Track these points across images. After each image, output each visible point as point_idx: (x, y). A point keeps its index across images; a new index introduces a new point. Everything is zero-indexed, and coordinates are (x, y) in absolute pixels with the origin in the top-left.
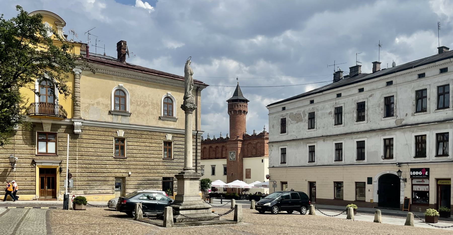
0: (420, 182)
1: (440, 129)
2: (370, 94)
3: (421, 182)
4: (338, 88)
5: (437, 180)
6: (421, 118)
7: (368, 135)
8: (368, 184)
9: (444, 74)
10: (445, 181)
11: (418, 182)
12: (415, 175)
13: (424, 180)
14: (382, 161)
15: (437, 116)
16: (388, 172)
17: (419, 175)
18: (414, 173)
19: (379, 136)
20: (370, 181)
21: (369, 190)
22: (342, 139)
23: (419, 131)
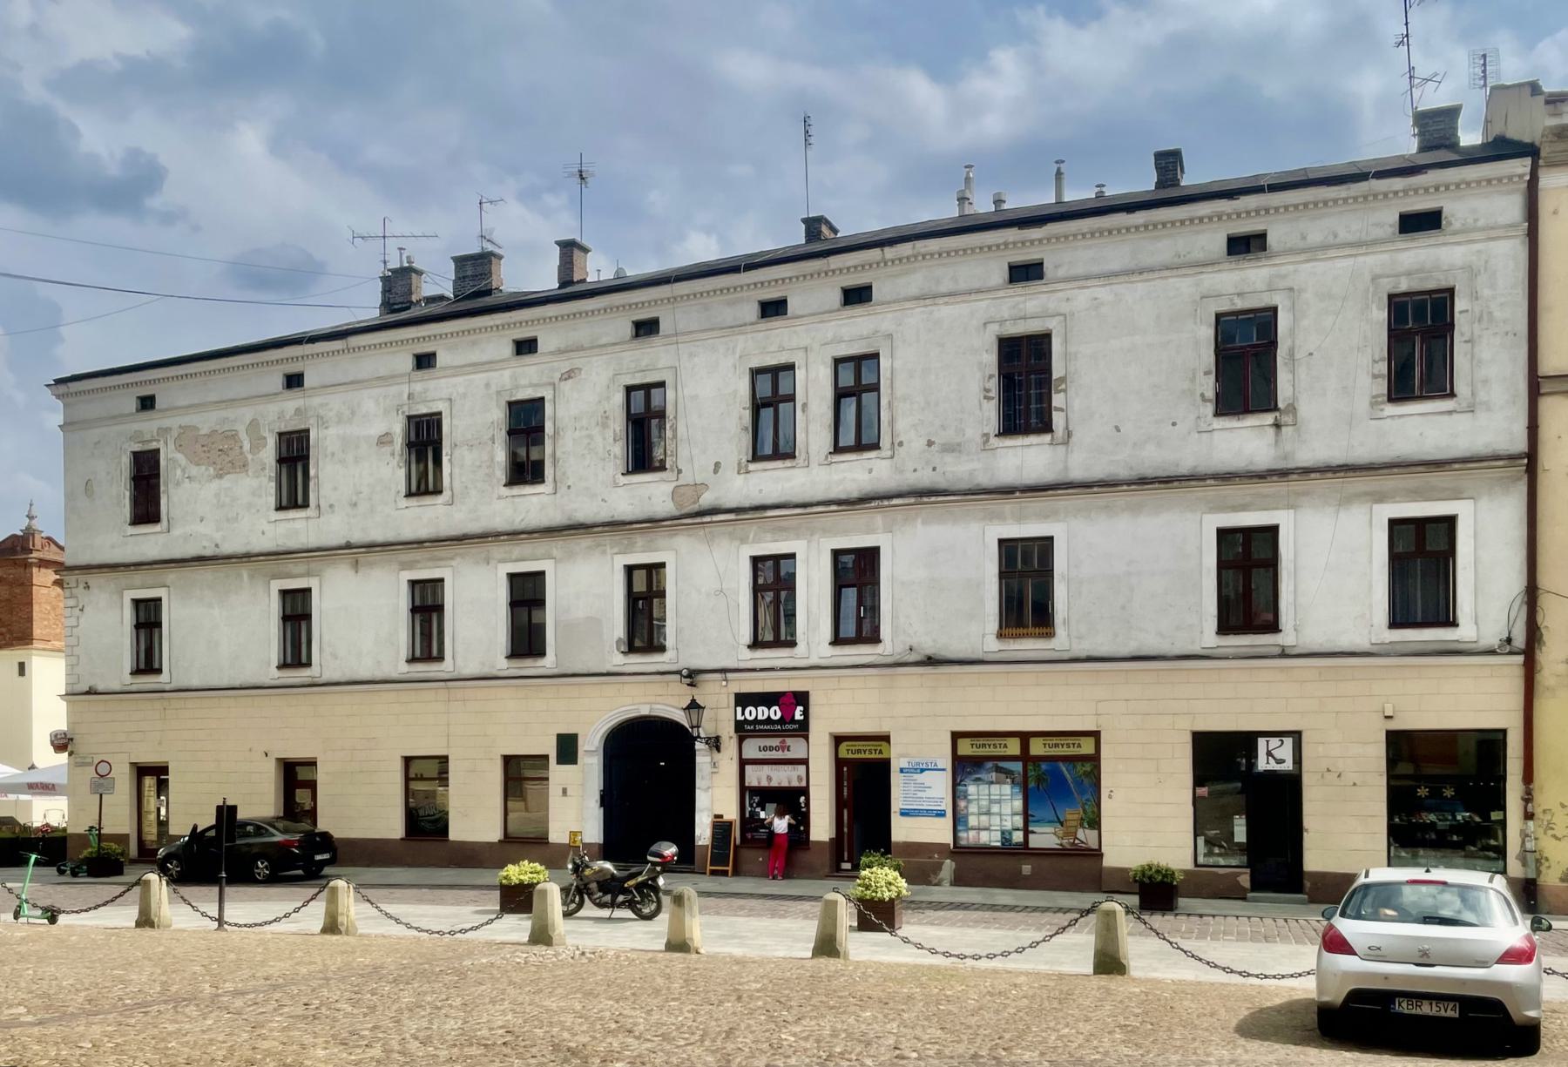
0: (771, 748)
2: (565, 366)
3: (777, 749)
6: (773, 482)
7: (557, 546)
8: (559, 762)
11: (765, 749)
12: (756, 722)
13: (789, 741)
14: (618, 661)
16: (645, 711)
17: (769, 721)
18: (751, 713)
20: (568, 748)
23: (769, 536)
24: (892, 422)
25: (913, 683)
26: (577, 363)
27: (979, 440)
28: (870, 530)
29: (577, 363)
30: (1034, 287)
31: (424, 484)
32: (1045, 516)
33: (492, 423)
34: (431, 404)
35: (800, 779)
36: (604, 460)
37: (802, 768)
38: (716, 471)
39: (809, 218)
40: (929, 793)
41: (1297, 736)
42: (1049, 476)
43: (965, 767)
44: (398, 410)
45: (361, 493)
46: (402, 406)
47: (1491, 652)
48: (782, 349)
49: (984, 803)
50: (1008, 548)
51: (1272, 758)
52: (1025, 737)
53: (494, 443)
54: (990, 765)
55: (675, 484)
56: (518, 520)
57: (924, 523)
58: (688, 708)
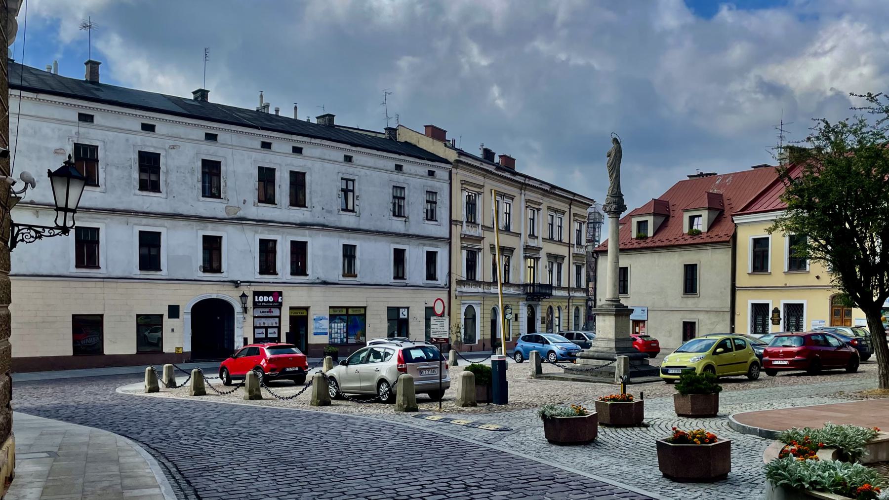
0: (265, 312)
1: (296, 235)
2: (172, 143)
3: (268, 312)
4: (90, 103)
5: (291, 308)
6: (266, 212)
7: (168, 222)
8: (170, 317)
9: (209, 142)
10: (298, 311)
11: (263, 312)
12: (263, 302)
13: (272, 309)
14: (201, 275)
15: (291, 214)
16: (214, 296)
17: (268, 302)
18: (261, 299)
19: (193, 228)
20: (174, 311)
21: (173, 330)
22: (99, 219)
23: (267, 232)
24: (311, 199)
25: (318, 291)
26: (178, 143)
27: (337, 211)
28: (304, 236)
29: (178, 143)
30: (151, 134)
31: (398, 211)
32: (354, 239)
33: (130, 159)
34: (92, 141)
35: (276, 323)
36: (192, 188)
37: (277, 320)
38: (244, 203)
39: (295, 120)
40: (323, 327)
41: (408, 308)
42: (355, 226)
43: (332, 318)
44: (69, 139)
45: (42, 176)
46: (72, 137)
47: (443, 287)
48: (270, 162)
49: (336, 330)
50: (396, 250)
51: (403, 314)
52: (347, 308)
53: (131, 168)
54: (338, 317)
55: (226, 205)
56: (145, 207)
57: (322, 236)
58: (241, 297)
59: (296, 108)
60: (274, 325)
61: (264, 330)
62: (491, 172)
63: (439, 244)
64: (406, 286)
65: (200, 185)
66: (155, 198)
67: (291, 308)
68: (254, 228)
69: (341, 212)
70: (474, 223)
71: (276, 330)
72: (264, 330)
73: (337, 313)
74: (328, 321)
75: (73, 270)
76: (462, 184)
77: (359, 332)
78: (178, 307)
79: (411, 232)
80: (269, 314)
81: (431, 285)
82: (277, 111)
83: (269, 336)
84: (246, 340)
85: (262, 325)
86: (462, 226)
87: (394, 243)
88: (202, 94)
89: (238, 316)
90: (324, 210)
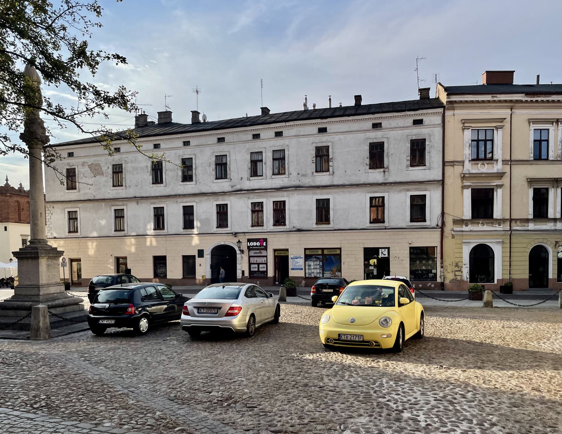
0: (257, 253)
1: (277, 197)
3: (259, 253)
7: (197, 199)
11: (255, 253)
12: (253, 246)
13: (262, 251)
16: (223, 243)
18: (252, 244)
23: (256, 197)
25: (295, 237)
28: (283, 196)
32: (328, 194)
35: (265, 261)
38: (241, 180)
40: (298, 264)
41: (388, 248)
43: (307, 257)
52: (323, 249)
54: (314, 256)
59: (330, 99)
60: (264, 262)
61: (256, 266)
62: (521, 101)
63: (428, 187)
64: (385, 229)
65: (214, 173)
66: (190, 185)
67: (275, 250)
68: (247, 195)
69: (315, 174)
70: (492, 159)
71: (265, 266)
72: (256, 266)
73: (312, 253)
74: (303, 260)
75: (315, 226)
76: (464, 123)
77: (334, 269)
78: (203, 250)
79: (391, 180)
80: (259, 255)
81: (420, 227)
82: (314, 106)
83: (261, 270)
84: (243, 272)
85: (255, 262)
86: (463, 165)
87: (369, 192)
88: (265, 110)
89: (239, 256)
90: (300, 175)
